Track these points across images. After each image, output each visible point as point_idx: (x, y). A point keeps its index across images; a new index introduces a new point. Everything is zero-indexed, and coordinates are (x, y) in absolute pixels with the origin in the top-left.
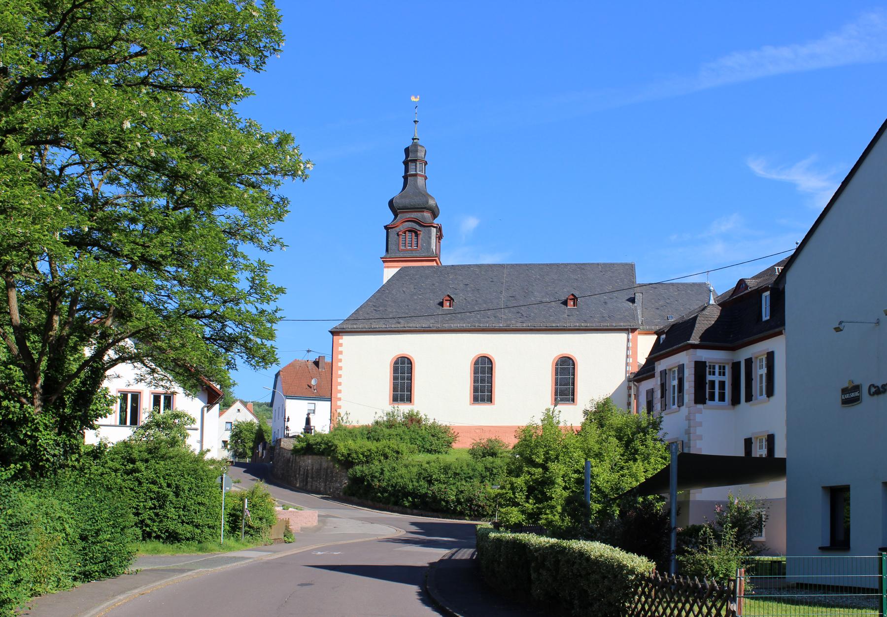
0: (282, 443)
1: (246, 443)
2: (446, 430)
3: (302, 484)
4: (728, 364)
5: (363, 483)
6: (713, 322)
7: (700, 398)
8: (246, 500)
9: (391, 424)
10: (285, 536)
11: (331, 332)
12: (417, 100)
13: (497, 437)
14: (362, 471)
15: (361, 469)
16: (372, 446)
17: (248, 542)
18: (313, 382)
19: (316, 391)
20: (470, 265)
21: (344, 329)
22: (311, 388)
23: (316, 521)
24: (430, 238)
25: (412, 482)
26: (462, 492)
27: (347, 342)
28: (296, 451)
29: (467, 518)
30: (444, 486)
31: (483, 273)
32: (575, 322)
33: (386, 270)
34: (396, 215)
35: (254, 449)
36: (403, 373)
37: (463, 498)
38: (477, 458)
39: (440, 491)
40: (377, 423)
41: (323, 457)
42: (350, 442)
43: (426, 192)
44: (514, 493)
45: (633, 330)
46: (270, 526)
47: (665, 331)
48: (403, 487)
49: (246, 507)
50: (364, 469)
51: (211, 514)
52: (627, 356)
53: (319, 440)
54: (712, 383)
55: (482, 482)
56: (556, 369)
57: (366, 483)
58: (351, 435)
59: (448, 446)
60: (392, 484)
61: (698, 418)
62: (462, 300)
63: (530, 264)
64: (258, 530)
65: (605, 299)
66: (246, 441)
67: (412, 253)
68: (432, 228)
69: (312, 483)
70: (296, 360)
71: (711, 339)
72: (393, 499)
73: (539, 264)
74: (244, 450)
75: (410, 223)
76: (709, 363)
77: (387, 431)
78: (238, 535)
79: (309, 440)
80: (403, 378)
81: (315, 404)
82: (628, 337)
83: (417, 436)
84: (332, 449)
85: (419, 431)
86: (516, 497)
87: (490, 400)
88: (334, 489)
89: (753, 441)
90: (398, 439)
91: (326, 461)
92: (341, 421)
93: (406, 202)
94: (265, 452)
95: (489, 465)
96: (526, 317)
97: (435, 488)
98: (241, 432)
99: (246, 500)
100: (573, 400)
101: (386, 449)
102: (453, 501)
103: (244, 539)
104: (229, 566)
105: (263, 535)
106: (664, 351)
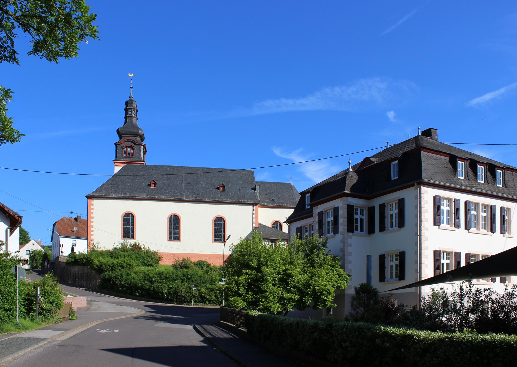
0: (59, 259)
1: (38, 261)
2: (156, 254)
4: (365, 208)
5: (110, 282)
6: (356, 181)
7: (351, 228)
8: (39, 288)
9: (124, 249)
10: (69, 315)
11: (86, 197)
12: (132, 76)
13: (188, 258)
14: (109, 275)
15: (109, 274)
16: (115, 261)
17: (42, 321)
18: (75, 229)
19: (76, 234)
20: (164, 166)
21: (94, 195)
22: (73, 232)
23: (86, 304)
24: (140, 151)
25: (141, 282)
26: (171, 288)
27: (96, 203)
28: (68, 263)
29: (175, 303)
30: (160, 284)
31: (172, 170)
32: (224, 199)
33: (116, 167)
34: (121, 138)
35: (42, 264)
36: (129, 222)
37: (172, 291)
38: (178, 269)
39: (158, 287)
40: (115, 248)
41: (85, 267)
42: (101, 258)
43: (137, 126)
44: (238, 288)
45: (256, 205)
46: (59, 308)
47: (310, 191)
48: (135, 284)
49: (39, 293)
50: (110, 274)
51: (6, 299)
52: (253, 218)
53: (82, 257)
54: (357, 219)
55: (182, 283)
56: (215, 224)
57: (112, 282)
59: (157, 263)
61: (350, 241)
62: (161, 184)
63: (197, 168)
64: (49, 311)
65: (239, 188)
66: (38, 260)
67: (130, 159)
68: (141, 146)
71: (356, 191)
72: (129, 291)
73: (202, 168)
74: (37, 265)
75: (129, 142)
76: (355, 206)
77: (123, 253)
78: (33, 316)
79: (76, 257)
80: (129, 225)
81: (76, 240)
83: (140, 256)
84: (90, 262)
85: (141, 254)
86: (240, 290)
87: (178, 239)
89: (386, 256)
90: (129, 257)
91: (86, 269)
92: (94, 247)
93: (127, 130)
94: (49, 265)
95: (185, 273)
96: (197, 195)
97: (155, 285)
98: (35, 255)
99: (39, 288)
101: (123, 263)
102: (166, 293)
103: (38, 318)
104: (22, 353)
105: (54, 316)
106: (318, 201)
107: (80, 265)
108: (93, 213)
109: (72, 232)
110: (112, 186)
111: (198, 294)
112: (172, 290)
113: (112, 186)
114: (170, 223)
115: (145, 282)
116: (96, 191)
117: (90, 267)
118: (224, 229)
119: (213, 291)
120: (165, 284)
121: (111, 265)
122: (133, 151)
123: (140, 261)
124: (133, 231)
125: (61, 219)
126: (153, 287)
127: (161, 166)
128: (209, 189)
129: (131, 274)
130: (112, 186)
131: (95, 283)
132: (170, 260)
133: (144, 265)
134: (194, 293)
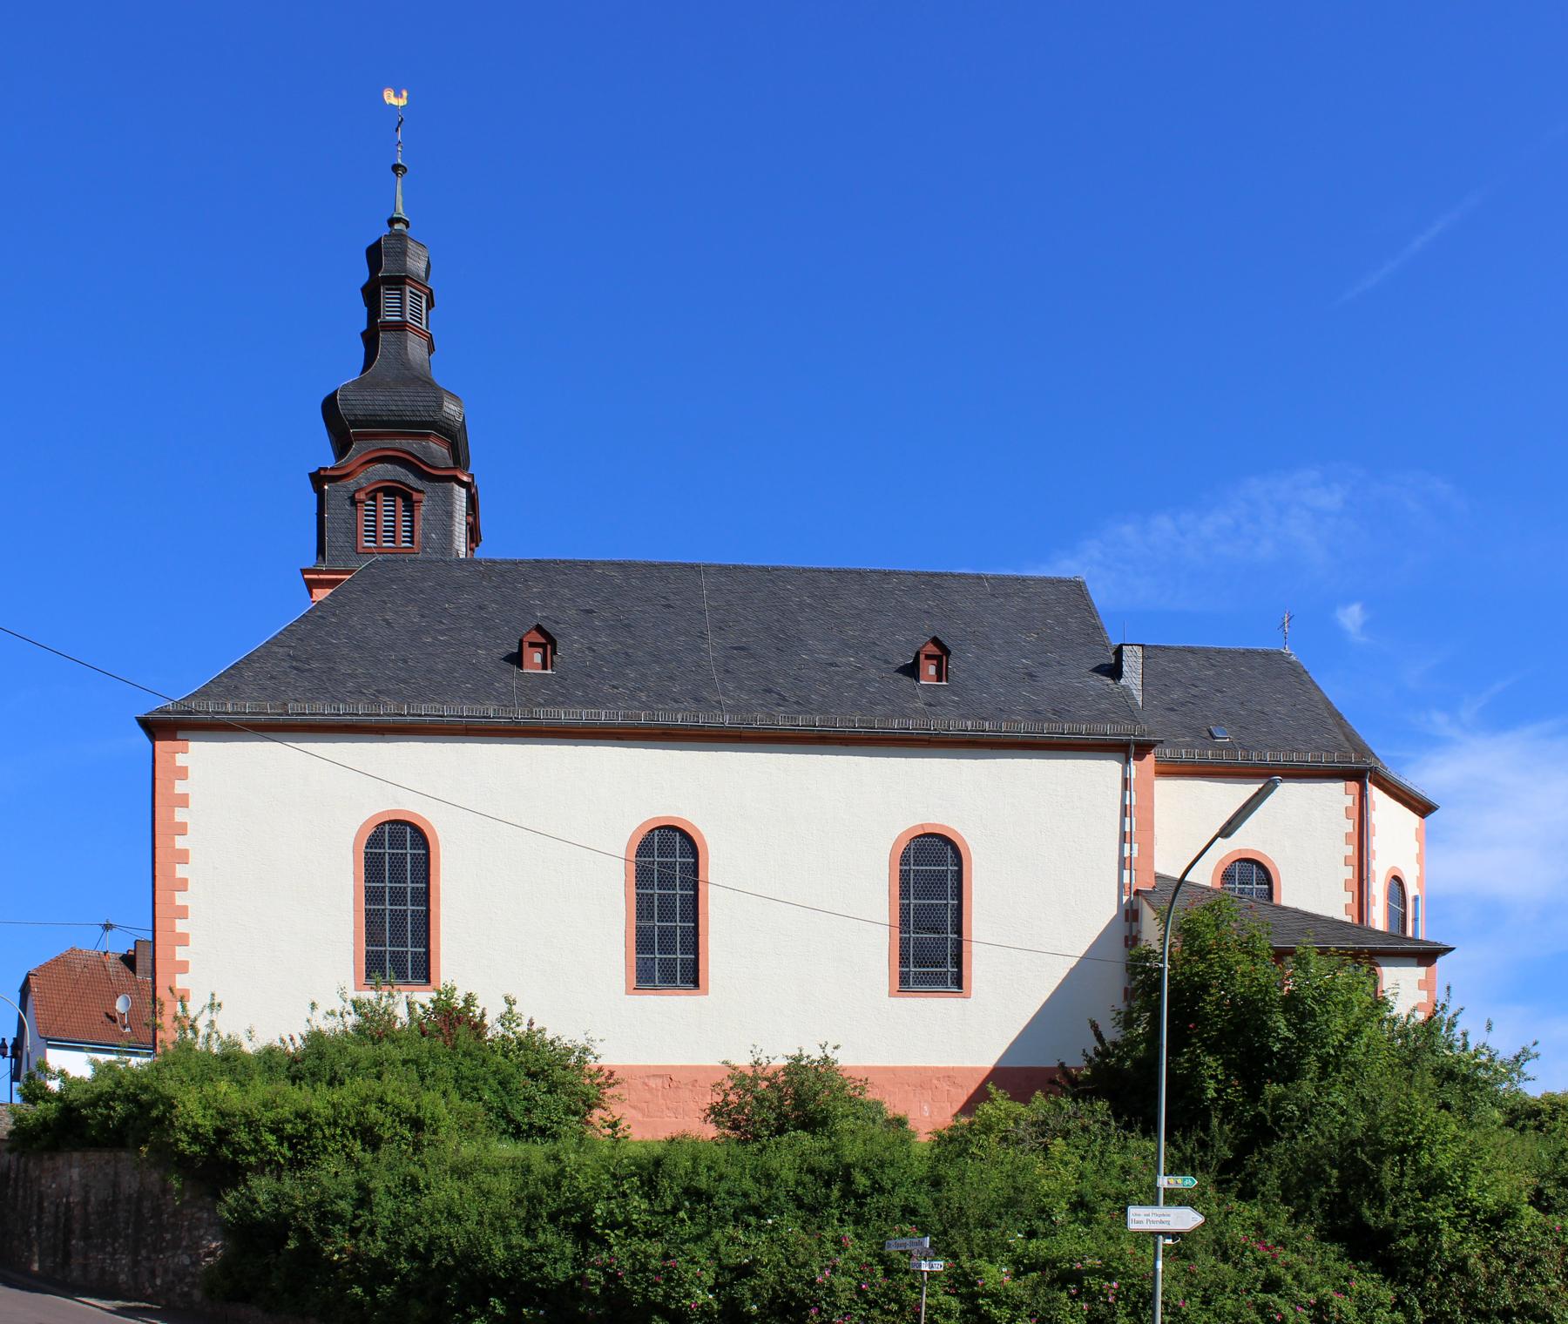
3: (49, 1263)
12: (402, 102)
13: (829, 1050)
16: (317, 1100)
18: (121, 1005)
19: (128, 1030)
22: (114, 1020)
24: (450, 515)
25: (506, 1232)
26: (744, 1271)
30: (656, 1248)
36: (397, 876)
37: (756, 1296)
39: (644, 1268)
41: (123, 1155)
42: (223, 1086)
45: (1142, 749)
56: (904, 877)
58: (225, 1065)
60: (413, 1247)
63: (775, 569)
68: (457, 487)
69: (86, 1257)
70: (73, 949)
80: (398, 896)
82: (1124, 772)
84: (154, 1113)
87: (690, 976)
88: (170, 1277)
92: (190, 1035)
93: (379, 402)
96: (797, 703)
97: (619, 1252)
100: (958, 981)
101: (373, 1110)
107: (95, 1144)
108: (182, 829)
109: (108, 1020)
110: (295, 668)
111: (960, 1307)
112: (753, 1289)
113: (295, 668)
114: (643, 876)
115: (535, 1237)
116: (204, 693)
117: (155, 1150)
118: (959, 910)
119: (1071, 1282)
120: (691, 1246)
121: (288, 1127)
122: (412, 516)
123: (480, 1099)
124: (423, 928)
125: (57, 960)
126: (603, 1269)
127: (572, 564)
128: (859, 676)
129: (427, 1187)
130: (294, 664)
131: (187, 1261)
132: (641, 1110)
133: (504, 1132)
134: (933, 1302)
